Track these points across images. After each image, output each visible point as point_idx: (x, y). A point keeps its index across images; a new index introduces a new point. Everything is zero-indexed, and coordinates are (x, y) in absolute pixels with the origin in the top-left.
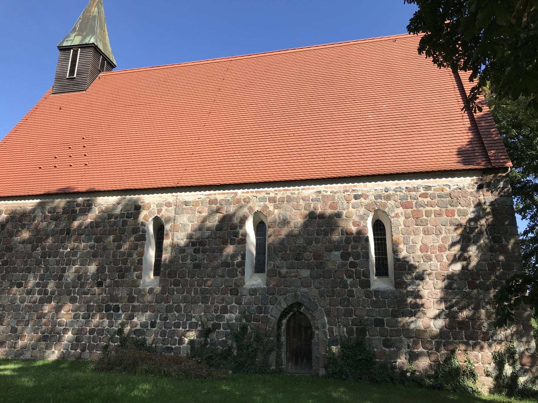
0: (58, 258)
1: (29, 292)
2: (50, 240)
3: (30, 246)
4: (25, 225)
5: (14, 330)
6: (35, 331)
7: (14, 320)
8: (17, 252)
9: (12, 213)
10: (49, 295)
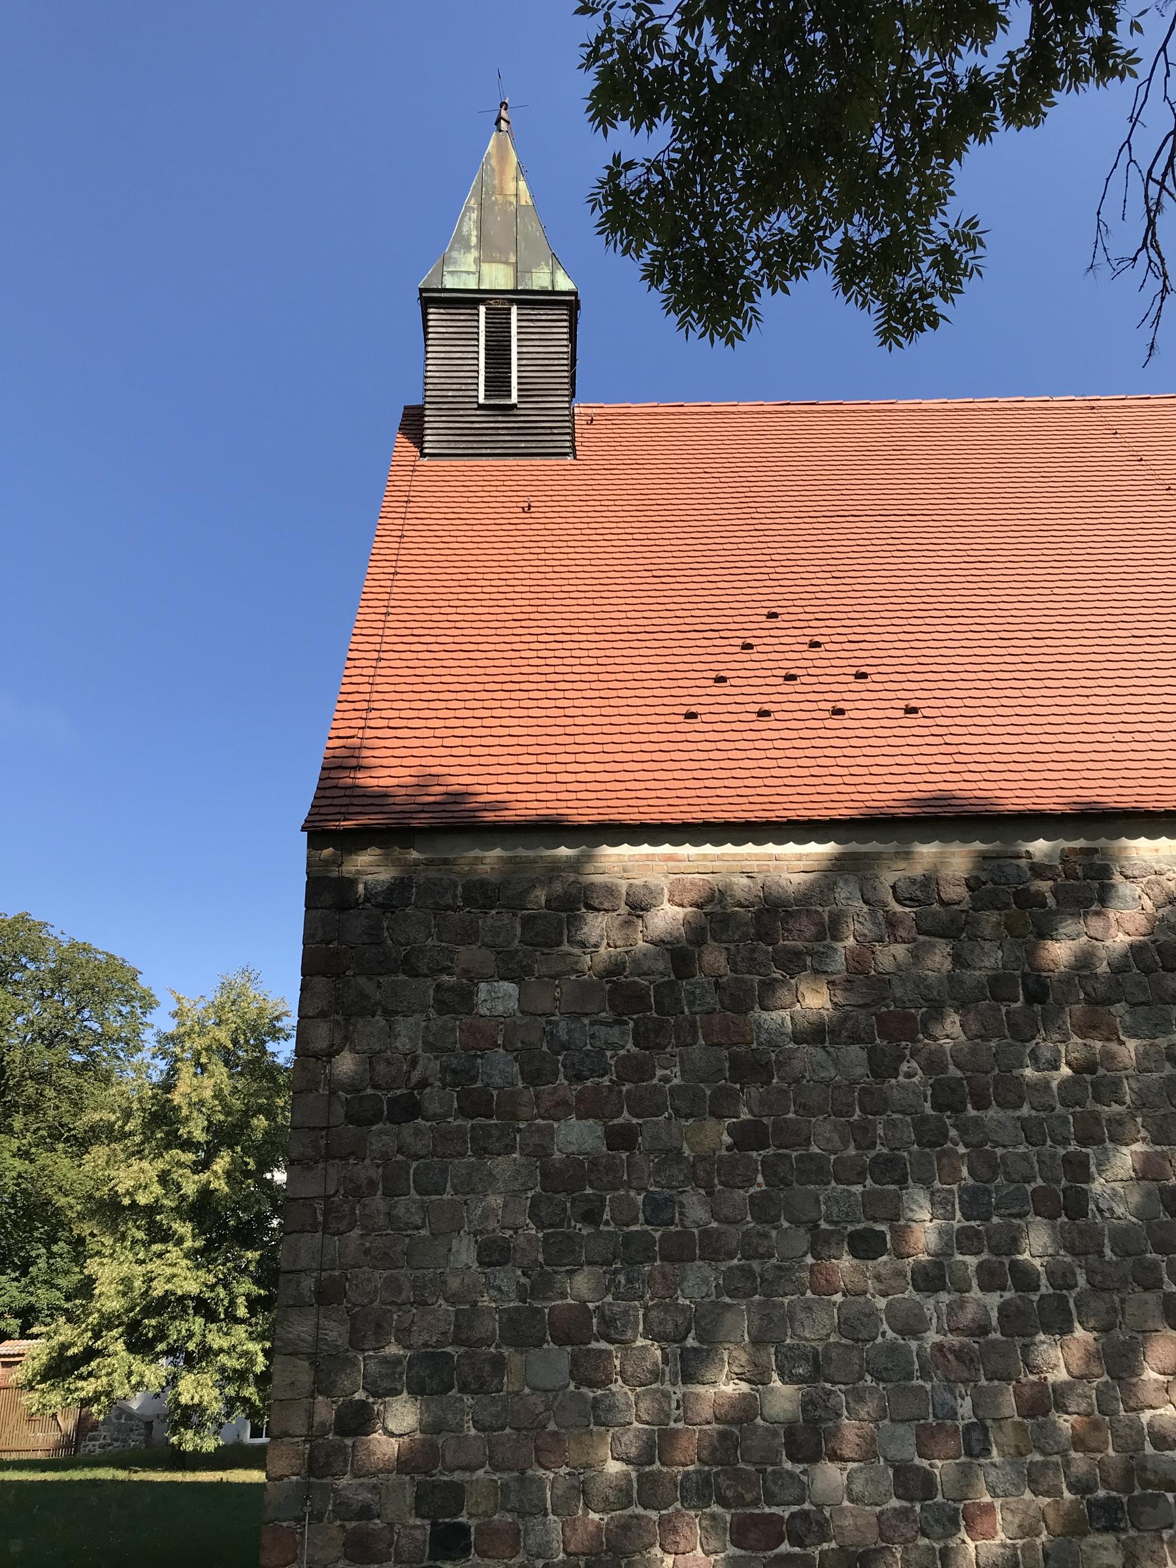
0: (1025, 1110)
1: (931, 1278)
2: (951, 1030)
3: (855, 1053)
4: (797, 954)
5: (913, 1483)
6: (1034, 1479)
7: (901, 1429)
8: (797, 1081)
9: (710, 899)
10: (1045, 1288)
